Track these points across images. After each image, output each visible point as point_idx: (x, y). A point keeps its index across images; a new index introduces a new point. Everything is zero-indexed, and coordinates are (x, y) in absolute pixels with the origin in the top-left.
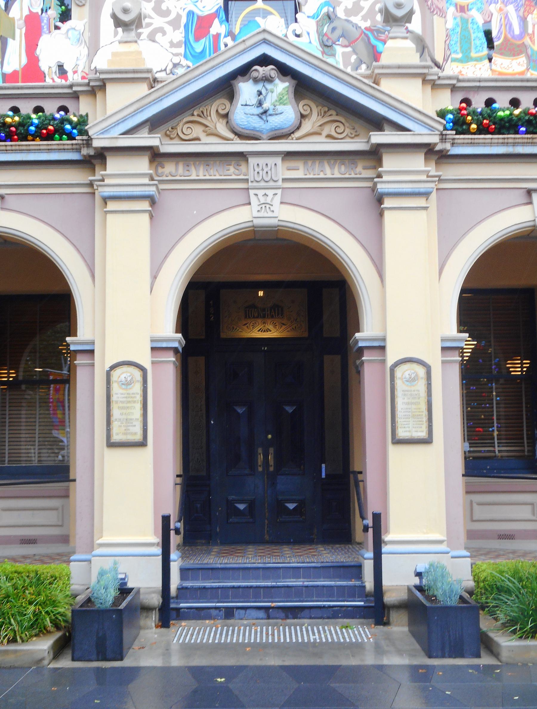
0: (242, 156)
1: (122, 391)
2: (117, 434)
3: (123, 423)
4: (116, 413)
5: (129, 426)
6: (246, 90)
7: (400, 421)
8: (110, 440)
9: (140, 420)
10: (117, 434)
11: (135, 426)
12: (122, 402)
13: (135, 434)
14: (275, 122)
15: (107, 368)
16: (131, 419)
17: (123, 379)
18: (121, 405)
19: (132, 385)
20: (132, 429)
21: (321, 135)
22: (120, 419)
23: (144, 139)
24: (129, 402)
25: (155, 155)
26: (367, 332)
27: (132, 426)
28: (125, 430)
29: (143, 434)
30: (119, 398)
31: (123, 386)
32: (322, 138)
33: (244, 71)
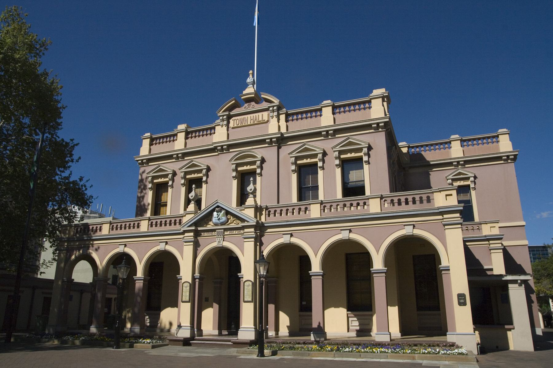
4: (184, 294)
6: (215, 214)
7: (245, 296)
14: (221, 221)
32: (233, 224)
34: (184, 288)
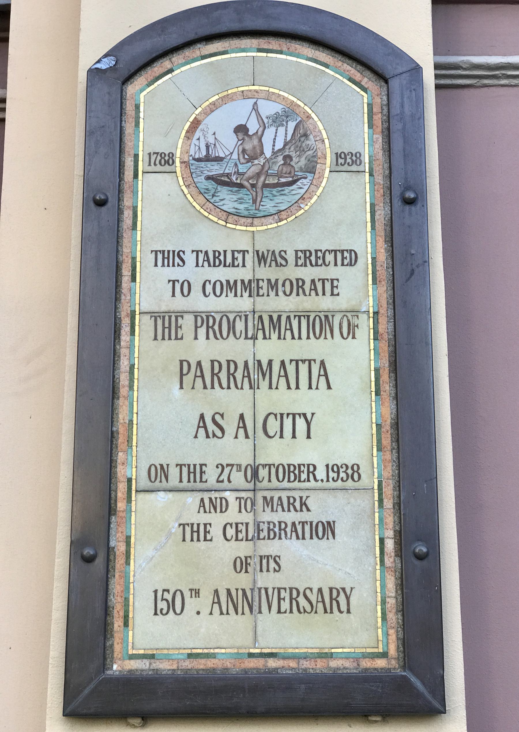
1: (215, 236)
2: (169, 603)
3: (219, 506)
5: (277, 531)
8: (105, 656)
9: (370, 478)
10: (169, 603)
11: (328, 529)
12: (210, 324)
13: (334, 600)
15: (94, 47)
16: (293, 472)
17: (228, 143)
18: (204, 349)
19: (297, 191)
20: (305, 563)
22: (196, 472)
24: (277, 324)
27: (297, 531)
28: (242, 565)
29: (404, 608)
30: (185, 288)
31: (228, 199)
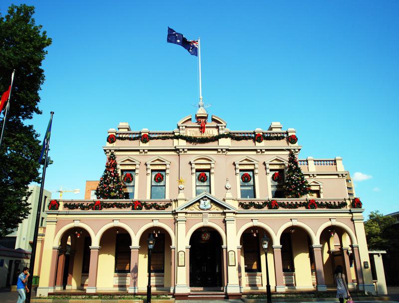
0: (201, 213)
6: (202, 201)
14: (207, 207)
21: (215, 209)
23: (184, 210)
25: (186, 213)
26: (224, 246)
33: (202, 198)
34: (179, 255)
